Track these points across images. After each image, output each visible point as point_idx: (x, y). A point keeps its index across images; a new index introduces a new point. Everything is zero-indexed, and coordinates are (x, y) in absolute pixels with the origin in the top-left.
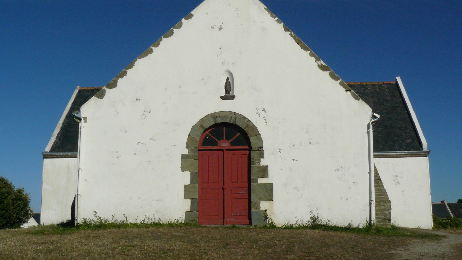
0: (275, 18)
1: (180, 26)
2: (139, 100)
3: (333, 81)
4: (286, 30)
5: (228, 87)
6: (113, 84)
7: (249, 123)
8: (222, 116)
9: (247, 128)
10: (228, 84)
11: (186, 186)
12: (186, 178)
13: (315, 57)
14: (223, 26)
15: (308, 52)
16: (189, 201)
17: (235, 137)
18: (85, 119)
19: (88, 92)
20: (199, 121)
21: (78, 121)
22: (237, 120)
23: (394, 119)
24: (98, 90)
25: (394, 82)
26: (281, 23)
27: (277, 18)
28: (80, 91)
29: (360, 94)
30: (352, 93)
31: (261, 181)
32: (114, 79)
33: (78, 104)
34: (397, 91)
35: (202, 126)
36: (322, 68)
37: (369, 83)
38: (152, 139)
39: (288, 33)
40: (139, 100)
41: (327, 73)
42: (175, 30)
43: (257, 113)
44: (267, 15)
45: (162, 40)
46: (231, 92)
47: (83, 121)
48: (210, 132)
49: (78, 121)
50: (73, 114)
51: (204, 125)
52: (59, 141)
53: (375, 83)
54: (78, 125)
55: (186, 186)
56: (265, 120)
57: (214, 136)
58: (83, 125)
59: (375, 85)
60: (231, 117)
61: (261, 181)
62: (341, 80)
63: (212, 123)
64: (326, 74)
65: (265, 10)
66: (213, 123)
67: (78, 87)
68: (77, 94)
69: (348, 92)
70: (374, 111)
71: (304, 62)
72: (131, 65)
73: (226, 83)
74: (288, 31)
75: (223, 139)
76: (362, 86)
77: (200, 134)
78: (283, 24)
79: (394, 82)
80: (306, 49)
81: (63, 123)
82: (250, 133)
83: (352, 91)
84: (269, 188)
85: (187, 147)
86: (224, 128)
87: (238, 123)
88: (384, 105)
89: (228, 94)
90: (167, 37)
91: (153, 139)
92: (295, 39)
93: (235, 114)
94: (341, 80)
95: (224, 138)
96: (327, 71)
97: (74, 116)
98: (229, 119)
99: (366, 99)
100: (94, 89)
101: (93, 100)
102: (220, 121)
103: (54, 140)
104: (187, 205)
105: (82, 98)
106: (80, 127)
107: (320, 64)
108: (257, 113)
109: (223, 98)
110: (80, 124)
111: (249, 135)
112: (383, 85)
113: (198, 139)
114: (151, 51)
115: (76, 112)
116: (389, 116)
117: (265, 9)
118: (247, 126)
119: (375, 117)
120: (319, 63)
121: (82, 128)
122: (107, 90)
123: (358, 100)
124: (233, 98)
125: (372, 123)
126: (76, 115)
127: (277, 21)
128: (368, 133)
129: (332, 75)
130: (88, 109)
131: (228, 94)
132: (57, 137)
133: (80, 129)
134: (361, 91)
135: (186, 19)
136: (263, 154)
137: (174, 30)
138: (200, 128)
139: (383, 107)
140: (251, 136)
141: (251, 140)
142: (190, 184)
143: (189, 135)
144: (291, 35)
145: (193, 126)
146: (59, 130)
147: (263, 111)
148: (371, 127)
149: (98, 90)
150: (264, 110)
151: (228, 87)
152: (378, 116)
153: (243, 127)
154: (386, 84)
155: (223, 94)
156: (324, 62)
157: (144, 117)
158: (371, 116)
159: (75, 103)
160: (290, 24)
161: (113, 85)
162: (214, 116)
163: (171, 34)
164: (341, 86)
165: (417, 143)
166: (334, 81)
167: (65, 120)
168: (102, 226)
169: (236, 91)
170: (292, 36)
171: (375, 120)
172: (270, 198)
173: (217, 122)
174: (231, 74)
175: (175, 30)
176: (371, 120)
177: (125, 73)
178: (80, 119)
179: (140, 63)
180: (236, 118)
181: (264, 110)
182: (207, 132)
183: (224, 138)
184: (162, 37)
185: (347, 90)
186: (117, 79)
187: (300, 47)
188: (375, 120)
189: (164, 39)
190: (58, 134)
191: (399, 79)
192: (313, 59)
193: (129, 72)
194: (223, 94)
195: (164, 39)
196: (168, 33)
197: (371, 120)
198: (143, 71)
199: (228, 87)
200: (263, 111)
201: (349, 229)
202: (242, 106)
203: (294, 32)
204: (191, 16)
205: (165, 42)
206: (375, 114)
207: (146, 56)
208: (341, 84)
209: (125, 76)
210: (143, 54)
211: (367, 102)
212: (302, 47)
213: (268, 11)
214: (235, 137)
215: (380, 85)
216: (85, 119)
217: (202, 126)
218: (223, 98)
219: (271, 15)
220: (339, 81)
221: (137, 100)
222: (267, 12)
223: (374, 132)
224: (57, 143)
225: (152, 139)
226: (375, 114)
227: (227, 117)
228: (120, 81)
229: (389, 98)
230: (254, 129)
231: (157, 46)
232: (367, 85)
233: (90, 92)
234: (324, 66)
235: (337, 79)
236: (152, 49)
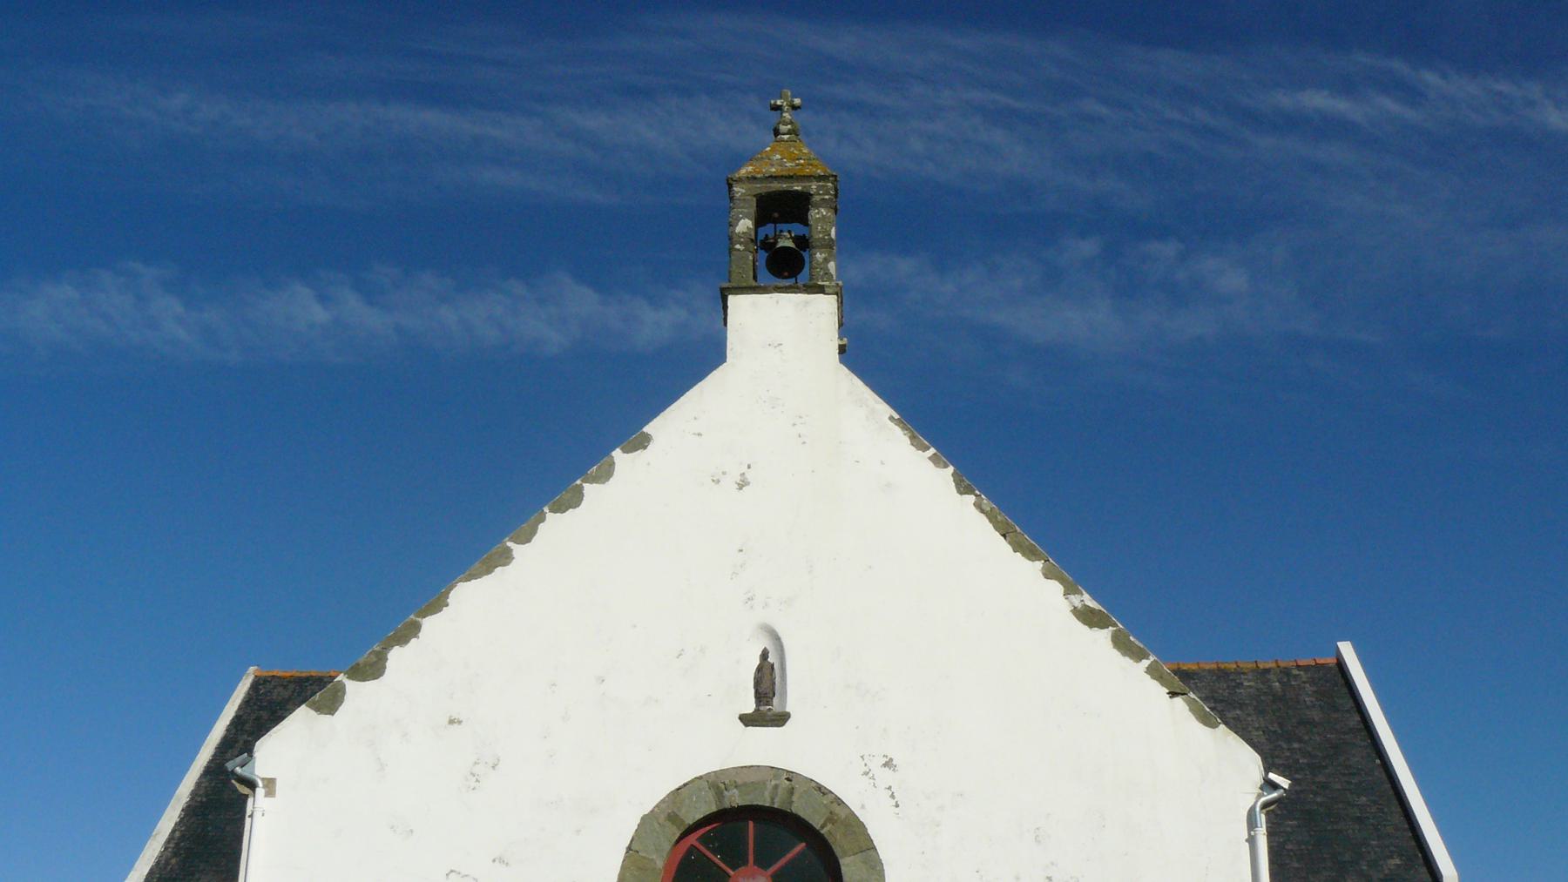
0: (926, 449)
1: (606, 474)
2: (460, 722)
3: (1127, 662)
4: (963, 489)
5: (767, 682)
6: (372, 665)
7: (837, 809)
8: (745, 784)
9: (829, 826)
10: (766, 671)
13: (1062, 581)
14: (750, 476)
15: (1039, 564)
17: (789, 856)
18: (270, 784)
19: (285, 687)
20: (663, 801)
21: (243, 790)
22: (795, 798)
23: (1338, 786)
24: (321, 682)
25: (1331, 661)
26: (946, 466)
27: (932, 451)
28: (255, 686)
29: (1216, 701)
30: (1190, 703)
32: (376, 648)
33: (247, 727)
34: (1345, 690)
35: (673, 818)
36: (1088, 617)
37: (1247, 665)
38: (500, 860)
39: (971, 499)
40: (460, 722)
41: (1103, 636)
42: (588, 488)
43: (866, 774)
44: (899, 439)
45: (543, 520)
46: (775, 700)
47: (260, 791)
48: (701, 839)
49: (243, 790)
50: (229, 765)
51: (682, 813)
52: (175, 854)
53: (1268, 666)
54: (245, 802)
56: (892, 796)
57: (715, 852)
58: (259, 804)
59: (1267, 671)
60: (776, 787)
62: (1152, 658)
63: (708, 807)
64: (1102, 638)
65: (891, 425)
66: (714, 809)
67: (252, 669)
68: (248, 693)
69: (1179, 700)
70: (1269, 767)
71: (1027, 599)
72: (435, 603)
73: (759, 669)
74: (972, 492)
75: (746, 862)
76: (1222, 674)
77: (667, 847)
78: (951, 469)
79: (1331, 661)
80: (1031, 554)
81: (194, 794)
82: (839, 843)
83: (1192, 695)
86: (751, 824)
87: (799, 808)
88: (1300, 740)
89: (767, 709)
90: (560, 508)
91: (502, 861)
92: (991, 518)
93: (790, 776)
94: (1152, 658)
95: (751, 858)
96: (1103, 626)
97: (233, 772)
98: (767, 794)
99: (1237, 719)
100: (307, 679)
101: (301, 719)
102: (736, 799)
103: (156, 854)
105: (261, 708)
106: (248, 812)
107: (1078, 604)
108: (866, 774)
109: (747, 720)
110: (250, 800)
111: (837, 851)
112: (1295, 672)
113: (660, 864)
114: (506, 558)
115: (238, 760)
116: (1321, 778)
117: (891, 418)
118: (831, 819)
119: (1274, 786)
120: (1076, 600)
121: (257, 815)
122: (351, 686)
123: (1214, 726)
124: (781, 719)
125: (1265, 806)
126: (238, 770)
127: (933, 459)
128: (1252, 840)
129: (1120, 643)
130: (273, 754)
131: (767, 709)
132: (169, 841)
133: (248, 820)
134: (1220, 695)
135: (626, 451)
137: (586, 486)
138: (668, 824)
139: (1296, 745)
140: (845, 854)
141: (844, 869)
143: (629, 848)
144: (978, 506)
145: (644, 819)
146: (176, 819)
147: (885, 765)
148: (1262, 819)
149: (321, 682)
150: (889, 764)
151: (767, 682)
152: (1284, 783)
153: (816, 822)
154: (1307, 668)
155: (750, 706)
156: (1094, 597)
157: (473, 784)
158: (1260, 781)
159: (237, 722)
160: (976, 472)
161: (371, 669)
162: (715, 782)
163: (576, 500)
164: (1153, 677)
165: (1424, 870)
167: (198, 784)
169: (794, 698)
170: (982, 511)
171: (1275, 795)
173: (727, 805)
174: (776, 639)
175: (588, 488)
176: (1259, 796)
177: (414, 629)
178: (252, 785)
179: (467, 596)
180: (791, 791)
181: (889, 764)
182: (692, 839)
183: (751, 858)
184: (546, 509)
185: (1173, 694)
186: (387, 647)
187: (1010, 548)
188: (1275, 795)
189: (550, 516)
190: (173, 831)
191: (1347, 650)
192: (1056, 587)
193: (429, 624)
194: (750, 706)
195: (550, 516)
196: (565, 496)
197: (1259, 796)
198: (475, 616)
199: (765, 685)
200: (885, 765)
202: (812, 750)
203: (989, 498)
204: (643, 442)
205: (554, 527)
206: (1272, 776)
207: (489, 571)
208: (1152, 671)
209: (413, 640)
210: (477, 564)
211: (1241, 729)
212: (1017, 547)
213: (904, 428)
214: (789, 856)
215: (1286, 672)
216: (270, 784)
217: (673, 818)
218: (747, 720)
219: (912, 438)
220: (1146, 663)
221: (452, 722)
222: (898, 430)
223: (1271, 834)
224: (167, 863)
225: (500, 860)
226: (1272, 776)
227: (758, 786)
228: (396, 656)
229: (1316, 715)
230: (855, 827)
231: (526, 538)
232: (1239, 672)
233: (292, 687)
234: (1092, 611)
235: (1138, 655)
236: (509, 550)
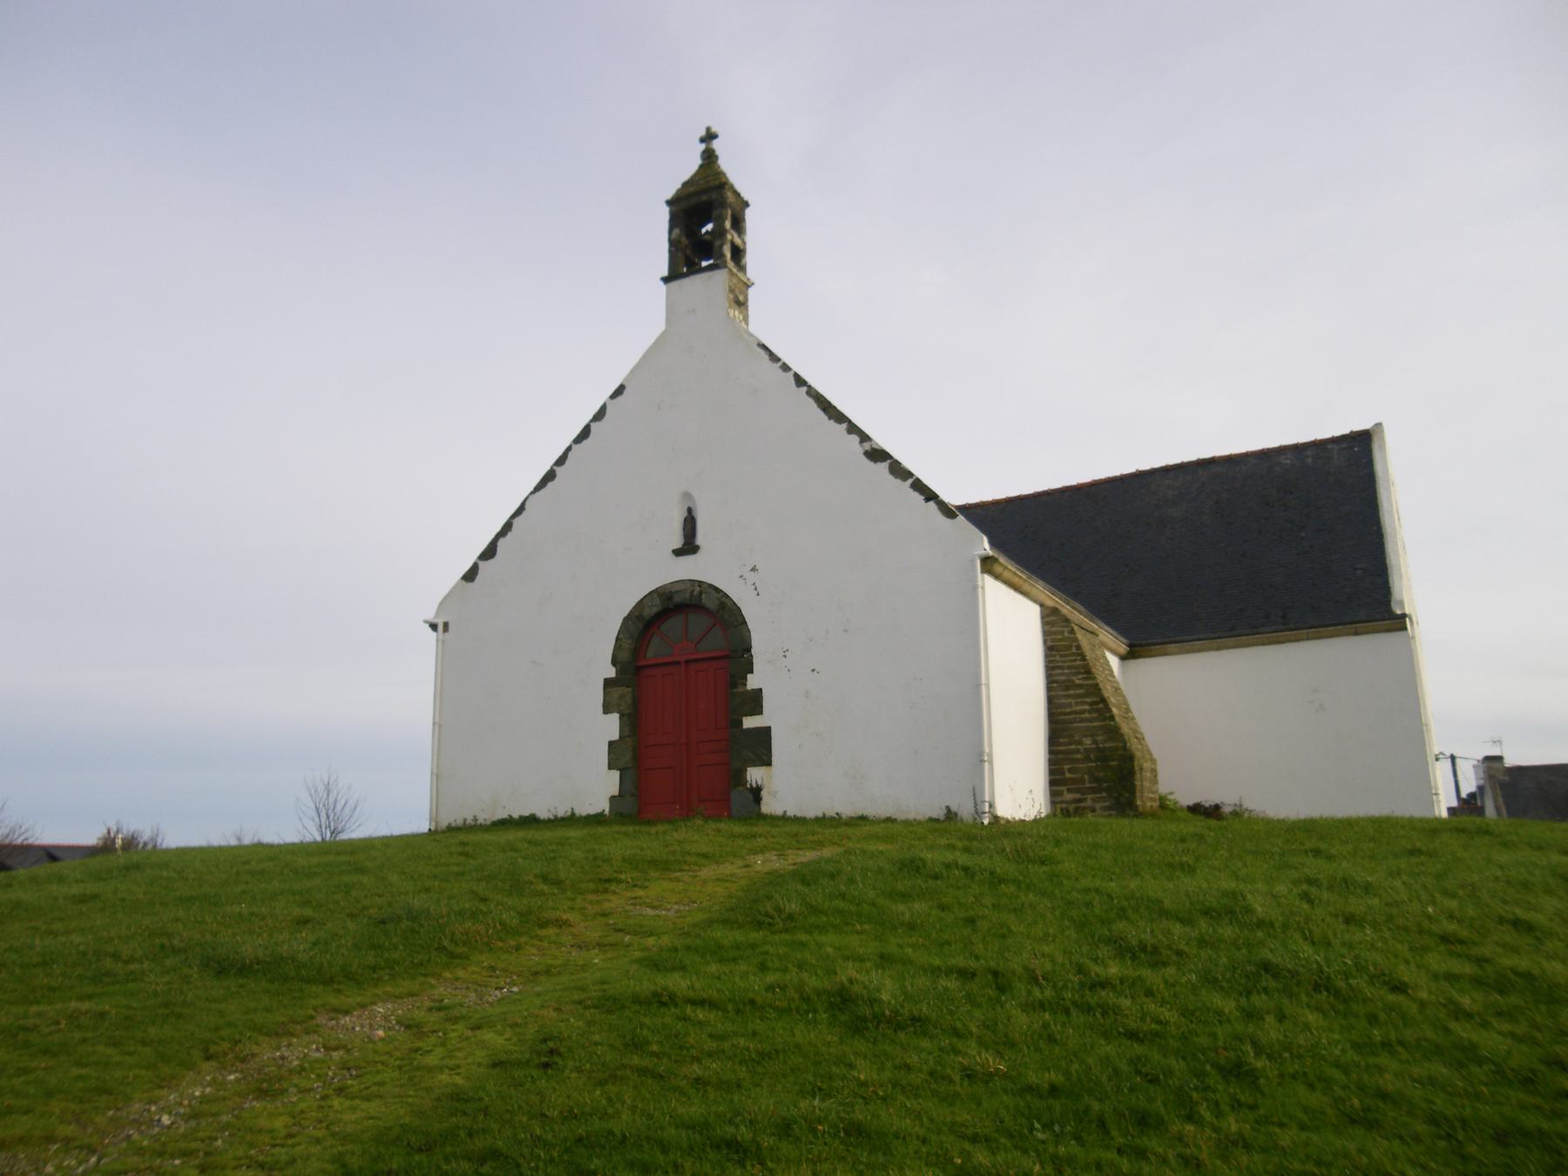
5: (690, 525)
11: (611, 744)
12: (611, 727)
16: (616, 774)
31: (749, 722)
55: (611, 744)
61: (749, 722)
84: (763, 736)
85: (614, 663)
89: (689, 547)
104: (610, 783)
109: (678, 553)
131: (689, 547)
136: (752, 663)
142: (597, 788)
145: (626, 620)
150: (754, 569)
151: (690, 525)
166: (898, 481)
168: (784, 819)
172: (767, 762)
201: (572, 820)
202: (709, 568)
